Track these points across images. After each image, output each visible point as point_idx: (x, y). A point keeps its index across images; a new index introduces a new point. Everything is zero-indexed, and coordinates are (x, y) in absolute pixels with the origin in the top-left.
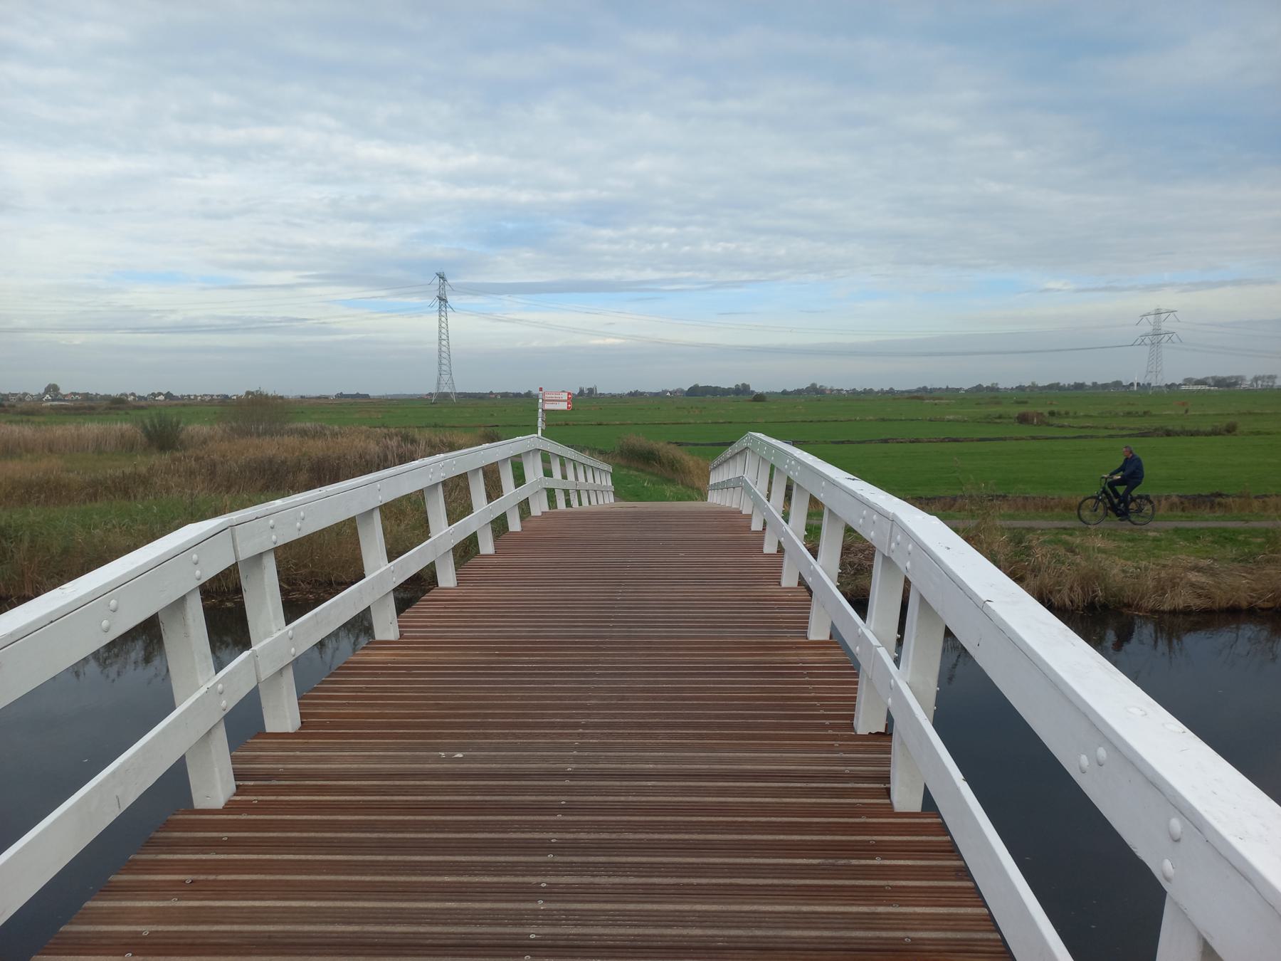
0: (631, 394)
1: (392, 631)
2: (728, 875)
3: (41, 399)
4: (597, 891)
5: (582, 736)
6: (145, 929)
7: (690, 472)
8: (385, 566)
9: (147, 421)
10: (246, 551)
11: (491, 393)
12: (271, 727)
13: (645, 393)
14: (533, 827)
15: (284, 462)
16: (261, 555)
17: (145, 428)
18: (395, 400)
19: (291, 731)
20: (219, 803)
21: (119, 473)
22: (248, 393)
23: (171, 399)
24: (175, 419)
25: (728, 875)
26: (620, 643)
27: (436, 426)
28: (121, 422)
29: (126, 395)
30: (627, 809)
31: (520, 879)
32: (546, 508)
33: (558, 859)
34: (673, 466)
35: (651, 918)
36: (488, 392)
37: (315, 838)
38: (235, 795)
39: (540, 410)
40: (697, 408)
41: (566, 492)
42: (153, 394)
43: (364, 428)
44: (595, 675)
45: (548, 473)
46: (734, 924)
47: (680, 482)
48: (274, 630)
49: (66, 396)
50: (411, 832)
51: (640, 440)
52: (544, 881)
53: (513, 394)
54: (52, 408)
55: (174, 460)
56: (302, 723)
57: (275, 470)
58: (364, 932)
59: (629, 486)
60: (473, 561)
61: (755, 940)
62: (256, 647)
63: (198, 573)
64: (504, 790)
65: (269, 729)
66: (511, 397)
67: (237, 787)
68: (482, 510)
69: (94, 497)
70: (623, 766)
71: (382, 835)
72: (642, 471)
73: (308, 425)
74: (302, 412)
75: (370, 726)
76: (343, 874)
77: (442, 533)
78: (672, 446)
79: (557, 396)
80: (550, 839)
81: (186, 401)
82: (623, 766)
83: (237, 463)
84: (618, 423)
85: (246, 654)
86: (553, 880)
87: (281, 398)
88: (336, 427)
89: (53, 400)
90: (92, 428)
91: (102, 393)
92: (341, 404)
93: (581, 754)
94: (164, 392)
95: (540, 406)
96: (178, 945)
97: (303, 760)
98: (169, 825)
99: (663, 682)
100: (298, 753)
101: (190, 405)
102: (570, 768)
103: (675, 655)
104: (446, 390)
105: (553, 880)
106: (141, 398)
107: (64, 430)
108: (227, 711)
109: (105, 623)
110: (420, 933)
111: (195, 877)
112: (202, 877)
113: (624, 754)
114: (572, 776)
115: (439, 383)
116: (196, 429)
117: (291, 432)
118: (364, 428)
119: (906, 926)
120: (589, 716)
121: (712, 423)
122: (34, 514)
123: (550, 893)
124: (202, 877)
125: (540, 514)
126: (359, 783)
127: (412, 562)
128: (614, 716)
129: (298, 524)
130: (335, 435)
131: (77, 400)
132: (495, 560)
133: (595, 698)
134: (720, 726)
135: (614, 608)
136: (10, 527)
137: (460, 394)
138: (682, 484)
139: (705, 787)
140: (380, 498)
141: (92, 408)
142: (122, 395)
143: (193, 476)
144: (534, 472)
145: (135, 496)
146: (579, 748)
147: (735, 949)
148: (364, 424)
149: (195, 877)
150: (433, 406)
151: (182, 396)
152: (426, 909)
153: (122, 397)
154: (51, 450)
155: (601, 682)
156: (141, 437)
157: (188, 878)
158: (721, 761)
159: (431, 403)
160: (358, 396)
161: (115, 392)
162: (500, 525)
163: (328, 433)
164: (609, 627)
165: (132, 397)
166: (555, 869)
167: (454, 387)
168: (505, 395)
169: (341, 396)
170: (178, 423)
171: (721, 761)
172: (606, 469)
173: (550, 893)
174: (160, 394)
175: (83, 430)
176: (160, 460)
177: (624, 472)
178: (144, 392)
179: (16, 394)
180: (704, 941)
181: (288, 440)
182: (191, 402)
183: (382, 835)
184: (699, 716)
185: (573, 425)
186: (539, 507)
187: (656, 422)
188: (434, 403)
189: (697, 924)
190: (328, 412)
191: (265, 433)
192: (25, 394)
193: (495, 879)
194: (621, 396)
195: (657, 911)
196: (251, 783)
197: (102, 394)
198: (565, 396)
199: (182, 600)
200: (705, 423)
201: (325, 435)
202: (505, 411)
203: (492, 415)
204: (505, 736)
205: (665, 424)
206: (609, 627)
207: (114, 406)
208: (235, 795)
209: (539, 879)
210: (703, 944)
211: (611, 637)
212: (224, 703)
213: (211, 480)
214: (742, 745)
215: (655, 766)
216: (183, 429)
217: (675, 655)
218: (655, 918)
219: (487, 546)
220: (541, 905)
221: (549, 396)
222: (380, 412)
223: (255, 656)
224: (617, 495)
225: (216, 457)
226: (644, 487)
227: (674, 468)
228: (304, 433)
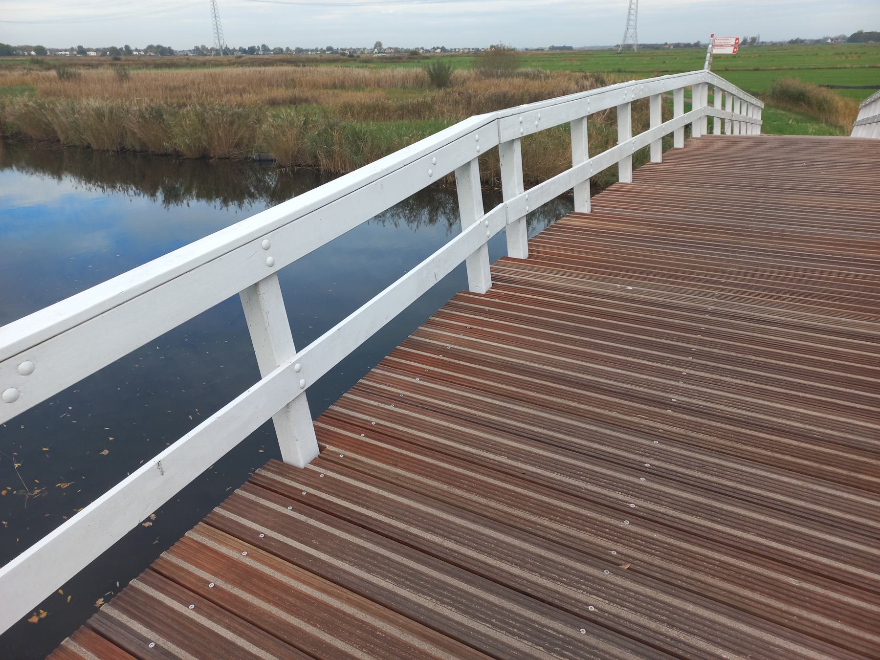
0: (792, 42)
1: (586, 206)
2: (830, 396)
3: (372, 52)
4: (723, 385)
5: (722, 290)
6: (449, 346)
7: (837, 111)
8: (587, 161)
9: (431, 67)
10: (506, 137)
11: (666, 44)
12: (511, 254)
13: (805, 40)
14: (679, 339)
15: (513, 97)
16: (513, 141)
17: (429, 71)
18: (591, 51)
19: (522, 258)
20: (483, 292)
21: (415, 101)
22: (492, 47)
23: (444, 52)
24: (447, 66)
25: (830, 396)
26: (758, 233)
27: (620, 71)
28: (416, 67)
29: (418, 49)
30: (752, 340)
31: (668, 367)
32: (705, 132)
33: (695, 360)
34: (821, 106)
35: (762, 409)
36: (664, 43)
37: (537, 319)
38: (491, 288)
39: (708, 55)
40: (856, 53)
41: (723, 121)
42: (434, 48)
43: (567, 72)
44: (735, 252)
45: (711, 102)
46: (830, 427)
47: (824, 121)
48: (518, 193)
49: (385, 50)
50: (596, 327)
51: (795, 82)
52: (685, 371)
53: (684, 44)
54: (378, 58)
55: (446, 94)
56: (529, 255)
57: (507, 102)
58: (566, 374)
59: (774, 123)
60: (645, 166)
61: (847, 440)
62: (505, 202)
63: (478, 147)
64: (659, 314)
65: (510, 256)
66: (681, 47)
67: (493, 284)
68: (657, 127)
69: (401, 117)
70: (752, 313)
71: (577, 325)
72: (790, 110)
73: (530, 69)
74: (526, 61)
75: (570, 262)
76: (553, 341)
77: (626, 142)
78: (823, 89)
79: (726, 41)
80: (691, 348)
81: (453, 53)
82: (752, 313)
83: (484, 96)
84: (774, 68)
85: (501, 205)
86: (691, 372)
87: (513, 50)
88: (548, 72)
89: (379, 53)
90: (400, 71)
91: (405, 48)
92: (552, 54)
93: (719, 301)
94: (441, 47)
95: (709, 50)
96: (465, 357)
97: (531, 275)
98: (456, 298)
99: (793, 264)
100: (527, 271)
101: (456, 56)
102: (710, 308)
103: (806, 246)
104: (630, 42)
105: (691, 372)
106: (427, 51)
107: (386, 72)
108: (490, 238)
109: (430, 171)
110: (599, 382)
111: (472, 326)
112: (475, 327)
113: (754, 306)
114: (712, 313)
115: (625, 37)
116: (460, 72)
117: (518, 75)
118: (567, 72)
119: (727, 595)
120: (728, 278)
121: (869, 67)
122: (372, 126)
123: (688, 378)
124: (475, 327)
125: (699, 136)
126: (564, 293)
127: (605, 160)
128: (749, 281)
129: (536, 122)
130: (547, 77)
131: (391, 52)
132: (662, 167)
133: (733, 267)
134: (840, 299)
135: (756, 208)
136: (361, 132)
137: (640, 45)
138: (826, 122)
139: (820, 337)
140: (589, 109)
141: (400, 58)
142: (416, 49)
143: (457, 105)
144: (700, 102)
145: (424, 117)
146: (719, 297)
147: (829, 442)
148: (568, 70)
149: (472, 326)
150: (619, 55)
151: (451, 49)
152: (604, 370)
153: (417, 50)
154: (379, 86)
155: (740, 257)
156: (427, 78)
157: (469, 326)
158: (837, 323)
159: (618, 53)
160: (564, 48)
161: (412, 47)
162: (667, 141)
163: (542, 75)
164: (750, 220)
165: (422, 50)
166: (693, 366)
167: (636, 39)
168: (677, 46)
169: (553, 48)
170: (449, 67)
171: (837, 323)
172: (759, 105)
173: (688, 378)
174: (438, 48)
175: (395, 72)
176: (439, 93)
177: (772, 111)
178: (428, 47)
179: (360, 49)
180: (803, 432)
181: (517, 81)
182: (456, 54)
183: (577, 325)
184: (823, 291)
185: (733, 70)
186: (700, 130)
187: (812, 67)
188: (620, 53)
189: (799, 420)
190: (543, 61)
191: (502, 75)
192: (365, 49)
193: (651, 363)
194: (781, 44)
195: (768, 406)
196: (501, 283)
197: (405, 48)
198: (733, 41)
199: (469, 164)
200: (862, 68)
201: (541, 77)
202: (675, 59)
203: (664, 62)
204: (663, 281)
205: (820, 69)
206: (750, 220)
207: (412, 56)
208: (491, 288)
209: (681, 370)
210: (802, 433)
211: (751, 228)
212: (488, 233)
213: (468, 108)
214: (859, 315)
215: (778, 317)
216: (452, 72)
217: (806, 246)
218: (765, 410)
219: (656, 156)
220: (681, 384)
221: (719, 41)
222: (579, 60)
223: (506, 207)
224: (763, 130)
225: (470, 91)
226: (788, 124)
227: (822, 108)
228: (526, 75)
